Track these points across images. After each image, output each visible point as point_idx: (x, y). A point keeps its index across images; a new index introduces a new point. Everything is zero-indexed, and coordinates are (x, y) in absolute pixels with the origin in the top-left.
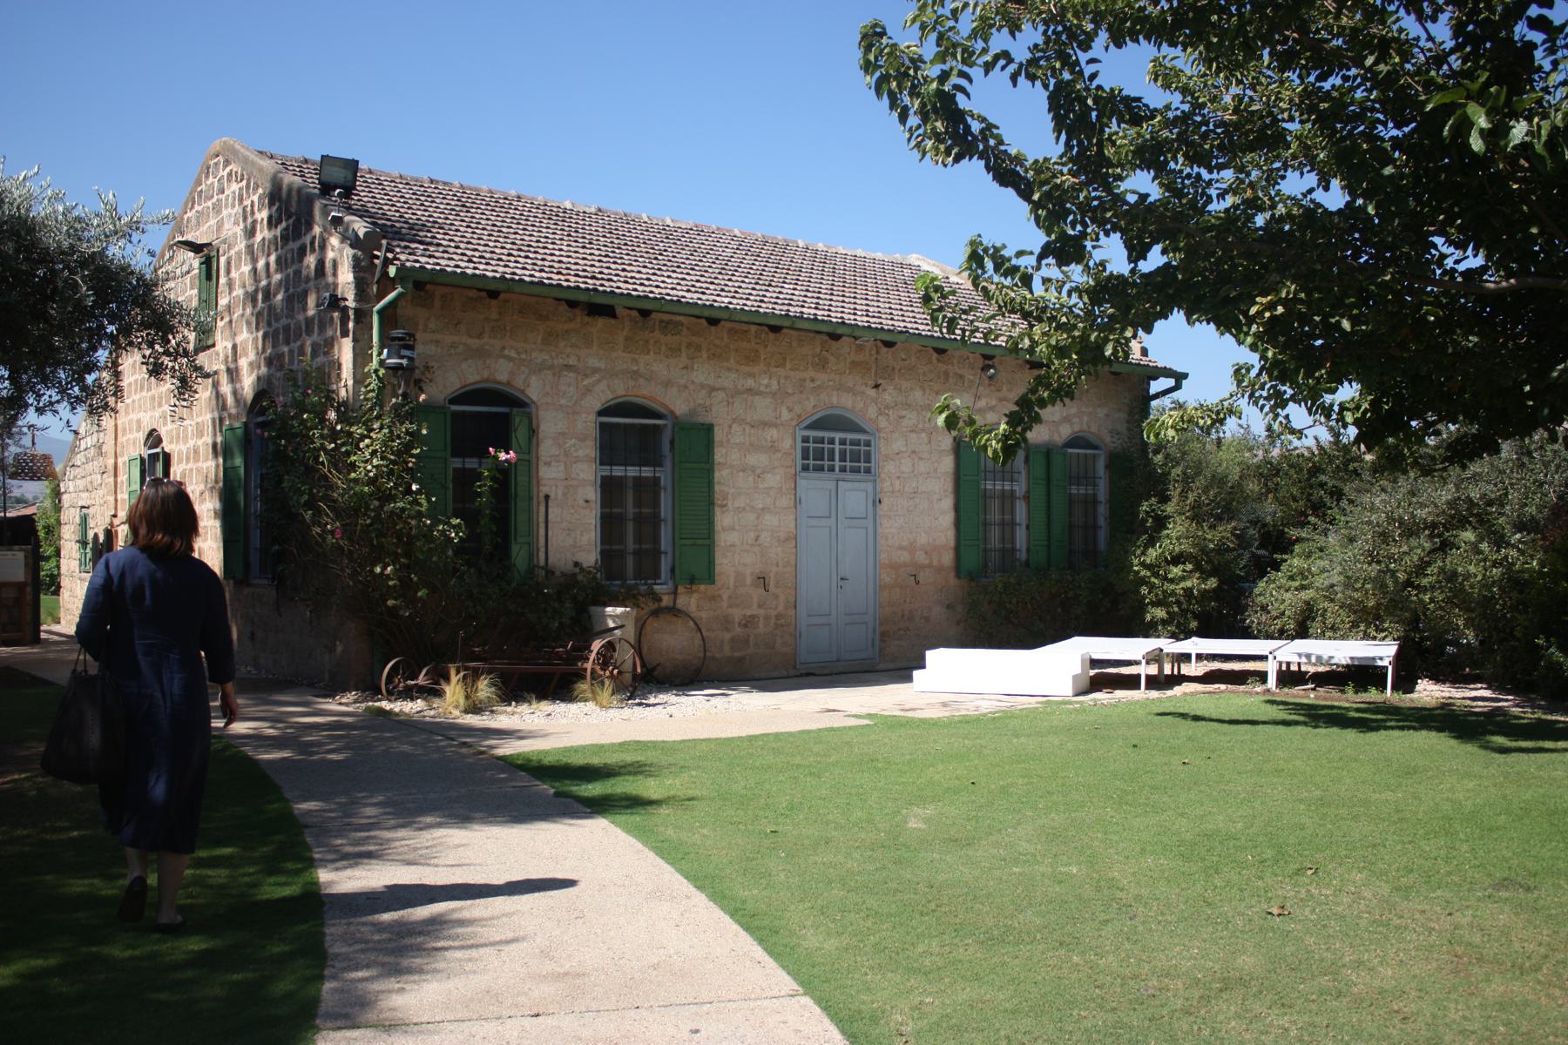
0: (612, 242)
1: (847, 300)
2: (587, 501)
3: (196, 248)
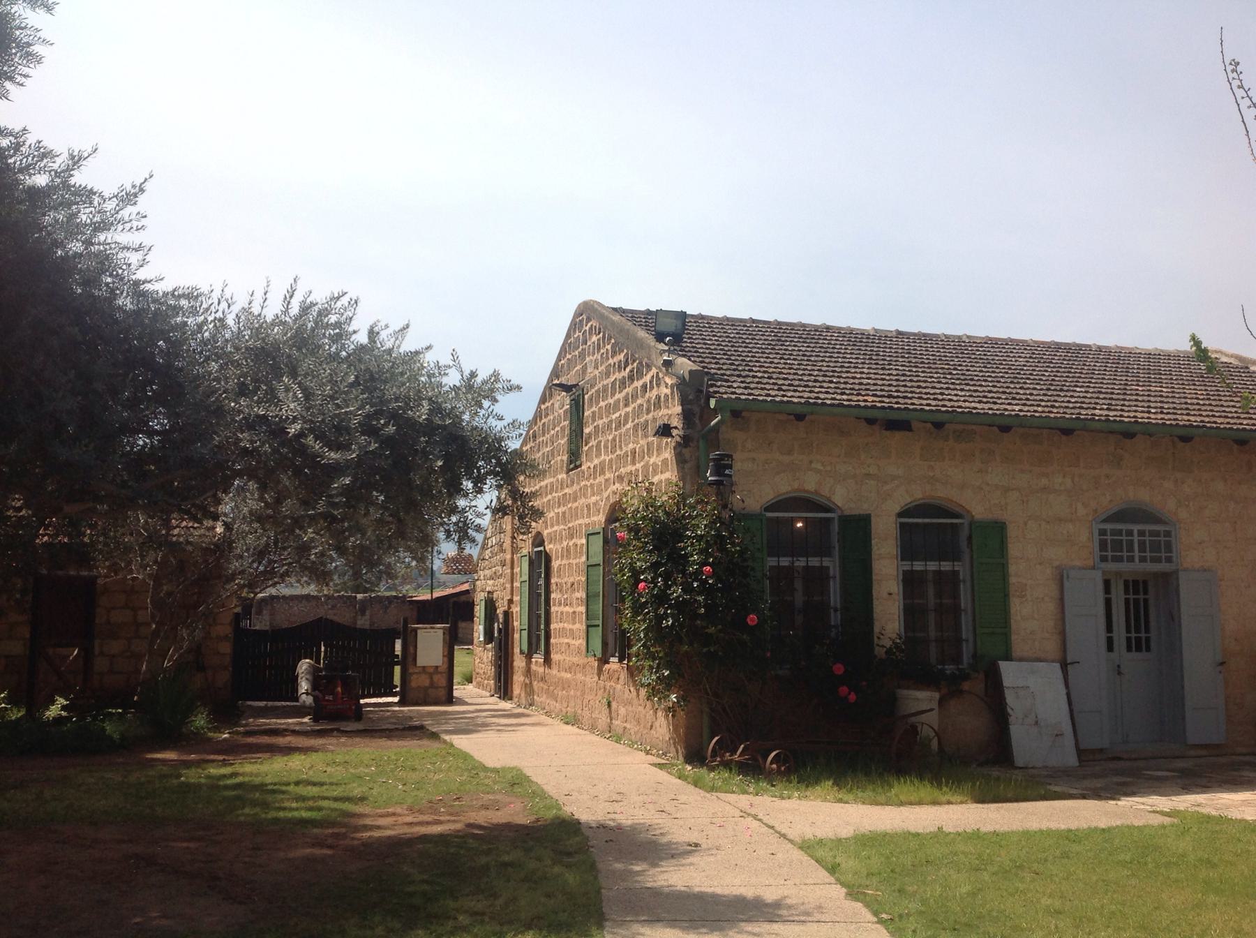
0: (909, 362)
1: (1140, 398)
2: (890, 594)
3: (567, 388)
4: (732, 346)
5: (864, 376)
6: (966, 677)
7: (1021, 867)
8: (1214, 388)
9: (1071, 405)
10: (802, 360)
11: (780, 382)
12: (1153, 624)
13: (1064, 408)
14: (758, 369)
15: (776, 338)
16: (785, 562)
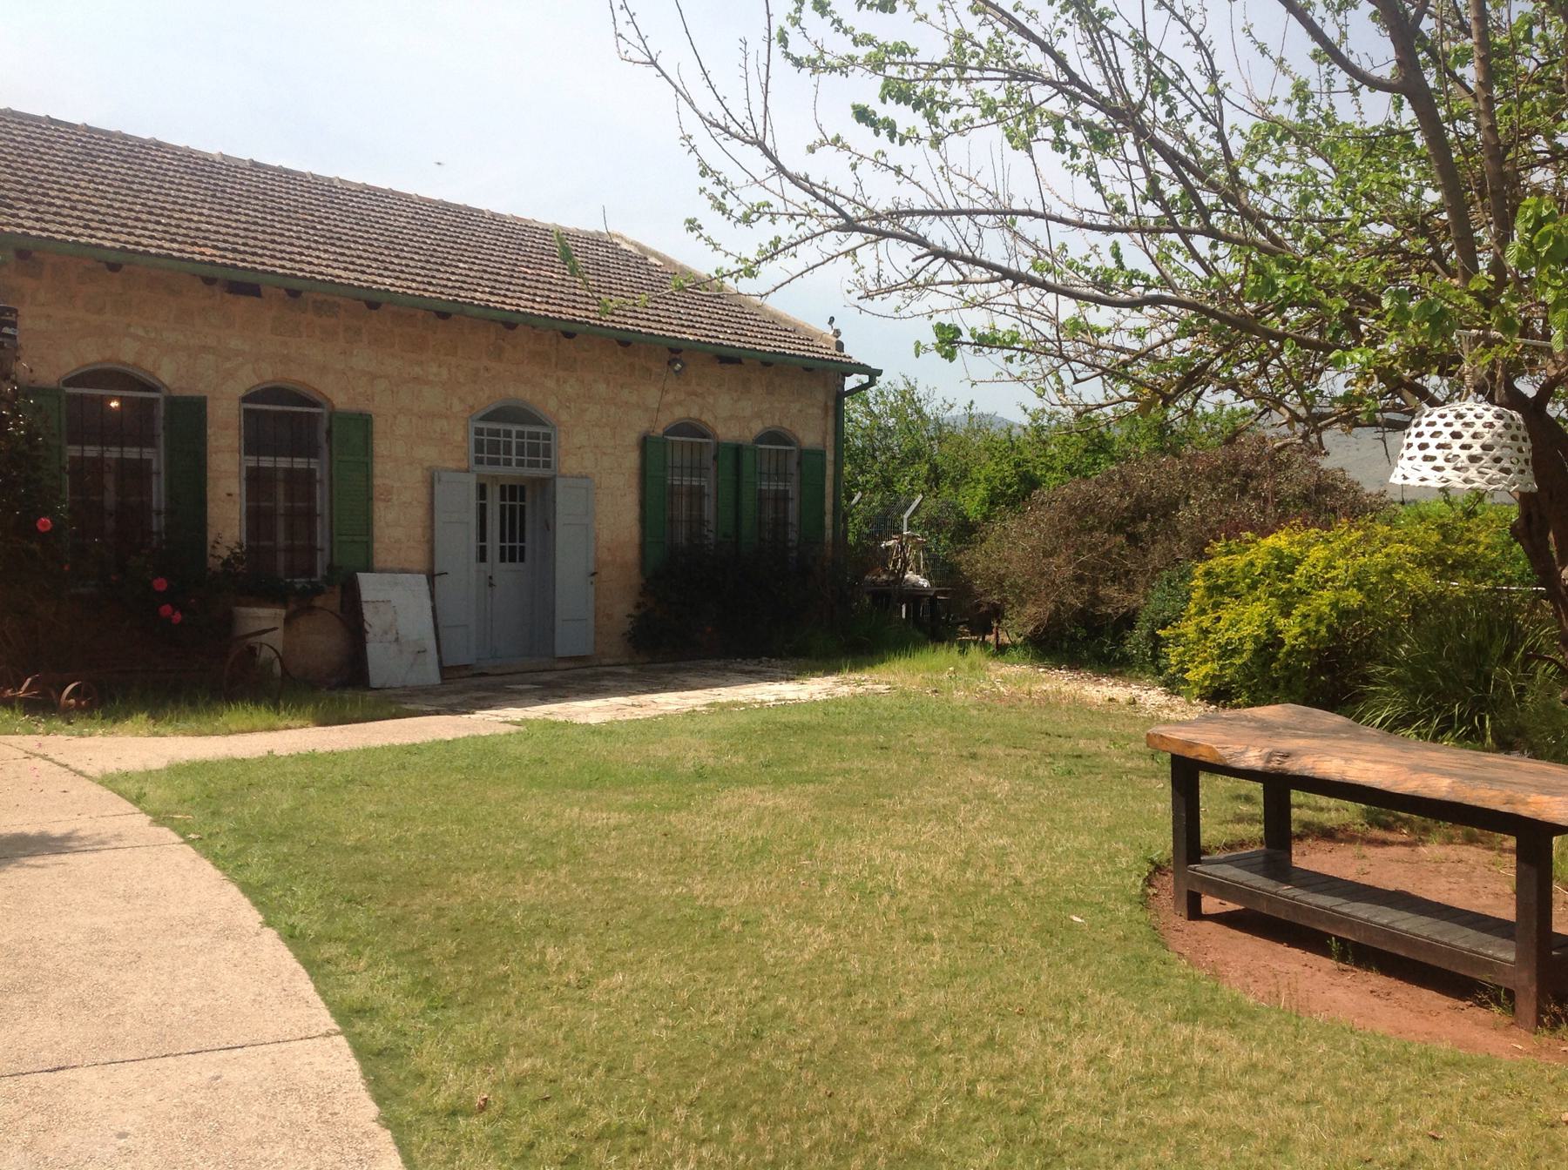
1: (527, 283)
2: (229, 495)
4: (19, 155)
5: (203, 219)
6: (317, 591)
7: (352, 781)
8: (607, 279)
9: (450, 284)
10: (119, 187)
11: (88, 216)
12: (528, 536)
13: (442, 288)
14: (56, 193)
15: (84, 151)
16: (91, 451)
